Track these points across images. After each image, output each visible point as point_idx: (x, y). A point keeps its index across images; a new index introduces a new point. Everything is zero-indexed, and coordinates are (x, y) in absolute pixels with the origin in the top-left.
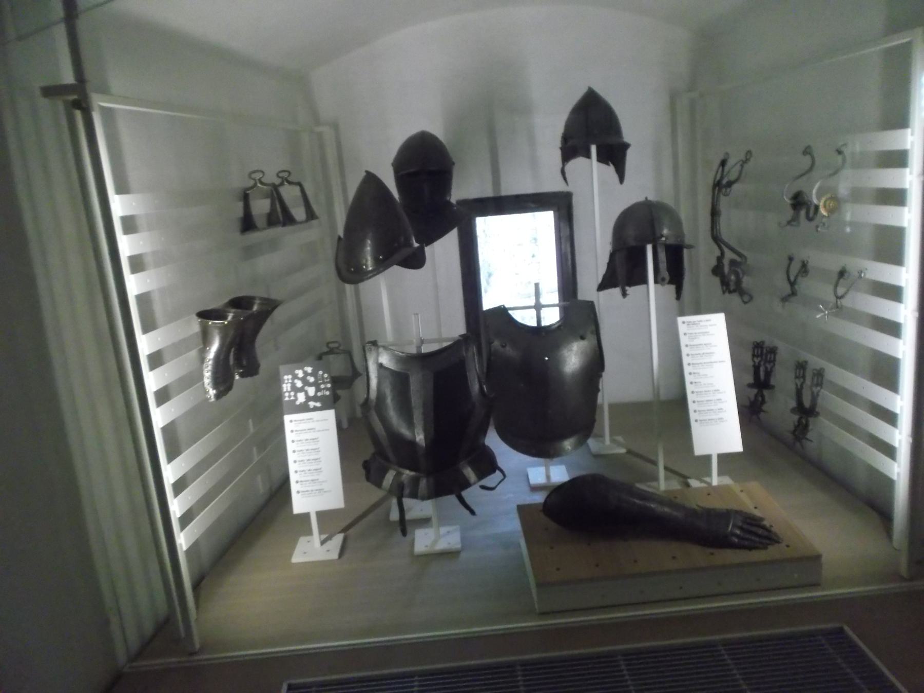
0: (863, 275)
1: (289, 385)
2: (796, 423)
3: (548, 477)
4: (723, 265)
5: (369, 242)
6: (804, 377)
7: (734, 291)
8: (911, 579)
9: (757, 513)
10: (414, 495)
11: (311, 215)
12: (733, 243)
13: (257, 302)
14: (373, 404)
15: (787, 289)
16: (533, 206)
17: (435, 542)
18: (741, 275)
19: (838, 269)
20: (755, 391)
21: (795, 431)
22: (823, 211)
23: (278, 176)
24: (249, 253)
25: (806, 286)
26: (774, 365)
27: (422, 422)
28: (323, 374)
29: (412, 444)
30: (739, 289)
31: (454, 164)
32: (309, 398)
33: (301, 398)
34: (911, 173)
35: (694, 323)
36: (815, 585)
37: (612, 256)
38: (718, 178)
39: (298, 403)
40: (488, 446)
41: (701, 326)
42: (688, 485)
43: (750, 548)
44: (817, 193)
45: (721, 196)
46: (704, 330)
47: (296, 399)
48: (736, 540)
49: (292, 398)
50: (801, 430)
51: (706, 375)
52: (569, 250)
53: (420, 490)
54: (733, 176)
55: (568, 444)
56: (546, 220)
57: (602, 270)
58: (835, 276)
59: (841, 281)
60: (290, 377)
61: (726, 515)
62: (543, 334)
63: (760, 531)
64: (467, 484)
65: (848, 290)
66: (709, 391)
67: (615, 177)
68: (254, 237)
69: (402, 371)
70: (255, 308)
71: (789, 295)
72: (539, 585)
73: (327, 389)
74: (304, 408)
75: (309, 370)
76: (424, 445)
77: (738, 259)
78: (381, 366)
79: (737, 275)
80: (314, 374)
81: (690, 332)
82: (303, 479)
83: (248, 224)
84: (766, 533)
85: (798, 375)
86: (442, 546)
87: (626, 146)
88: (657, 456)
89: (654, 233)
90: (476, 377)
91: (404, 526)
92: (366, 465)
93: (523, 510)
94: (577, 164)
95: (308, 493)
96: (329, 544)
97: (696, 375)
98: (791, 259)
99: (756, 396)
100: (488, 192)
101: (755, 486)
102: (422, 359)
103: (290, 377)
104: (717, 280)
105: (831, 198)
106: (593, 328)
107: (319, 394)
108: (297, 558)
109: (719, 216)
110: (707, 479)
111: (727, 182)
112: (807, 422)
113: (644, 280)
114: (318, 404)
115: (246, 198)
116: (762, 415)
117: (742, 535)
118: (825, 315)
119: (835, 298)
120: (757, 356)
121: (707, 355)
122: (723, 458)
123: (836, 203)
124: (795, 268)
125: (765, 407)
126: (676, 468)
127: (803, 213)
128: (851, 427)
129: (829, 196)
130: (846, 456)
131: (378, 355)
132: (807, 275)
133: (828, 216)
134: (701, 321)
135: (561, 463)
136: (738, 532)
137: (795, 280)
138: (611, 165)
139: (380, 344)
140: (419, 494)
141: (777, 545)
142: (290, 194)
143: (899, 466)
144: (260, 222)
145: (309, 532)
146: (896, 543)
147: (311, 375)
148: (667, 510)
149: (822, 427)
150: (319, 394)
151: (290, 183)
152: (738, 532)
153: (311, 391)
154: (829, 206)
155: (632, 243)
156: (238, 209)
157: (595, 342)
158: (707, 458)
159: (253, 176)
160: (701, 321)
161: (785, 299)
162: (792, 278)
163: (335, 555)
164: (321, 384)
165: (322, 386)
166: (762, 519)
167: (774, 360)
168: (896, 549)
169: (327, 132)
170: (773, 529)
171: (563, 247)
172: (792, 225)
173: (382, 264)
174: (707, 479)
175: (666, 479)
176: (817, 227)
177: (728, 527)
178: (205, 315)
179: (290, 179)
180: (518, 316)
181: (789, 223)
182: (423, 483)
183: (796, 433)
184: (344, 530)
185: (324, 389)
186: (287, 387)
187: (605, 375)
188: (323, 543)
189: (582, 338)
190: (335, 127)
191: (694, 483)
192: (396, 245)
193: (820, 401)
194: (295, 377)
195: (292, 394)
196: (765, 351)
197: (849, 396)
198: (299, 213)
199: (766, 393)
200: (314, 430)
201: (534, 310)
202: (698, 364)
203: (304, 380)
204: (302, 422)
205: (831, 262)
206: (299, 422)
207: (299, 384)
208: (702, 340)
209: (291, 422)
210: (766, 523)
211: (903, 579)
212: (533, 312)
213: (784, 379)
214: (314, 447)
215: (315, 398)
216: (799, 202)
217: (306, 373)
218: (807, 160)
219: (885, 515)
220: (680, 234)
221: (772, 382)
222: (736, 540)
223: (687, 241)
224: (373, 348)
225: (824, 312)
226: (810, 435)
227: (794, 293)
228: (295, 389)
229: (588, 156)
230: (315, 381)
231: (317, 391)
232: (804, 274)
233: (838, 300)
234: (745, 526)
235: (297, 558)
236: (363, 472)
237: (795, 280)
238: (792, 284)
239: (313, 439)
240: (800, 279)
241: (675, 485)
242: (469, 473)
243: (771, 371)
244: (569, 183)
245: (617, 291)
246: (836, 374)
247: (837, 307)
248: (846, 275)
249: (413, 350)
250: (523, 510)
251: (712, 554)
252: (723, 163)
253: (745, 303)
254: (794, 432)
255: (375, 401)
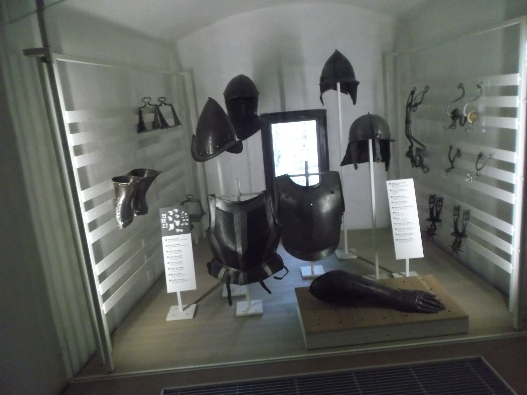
0: (492, 157)
1: (165, 220)
2: (454, 241)
3: (313, 272)
4: (413, 151)
5: (210, 138)
6: (458, 215)
7: (419, 166)
8: (520, 330)
9: (432, 292)
10: (236, 282)
11: (177, 122)
12: (418, 139)
13: (147, 172)
14: (213, 230)
15: (449, 165)
16: (304, 117)
17: (248, 309)
18: (423, 157)
19: (478, 153)
20: (431, 223)
21: (453, 246)
22: (469, 121)
23: (158, 100)
24: (142, 144)
25: (460, 163)
26: (442, 208)
27: (241, 241)
28: (184, 213)
29: (235, 253)
30: (421, 165)
31: (259, 93)
32: (176, 227)
33: (172, 227)
34: (520, 99)
35: (396, 184)
36: (465, 334)
37: (349, 146)
38: (410, 102)
39: (170, 230)
40: (278, 254)
41: (400, 186)
42: (392, 277)
43: (428, 313)
44: (466, 110)
45: (412, 112)
46: (401, 188)
47: (169, 227)
48: (420, 308)
49: (167, 227)
50: (457, 245)
51: (403, 214)
52: (324, 142)
53: (239, 279)
54: (418, 101)
55: (324, 253)
56: (311, 125)
57: (343, 154)
58: (476, 158)
59: (480, 160)
60: (165, 215)
61: (414, 294)
62: (310, 190)
63: (434, 303)
64: (266, 276)
65: (484, 166)
66: (404, 223)
67: (351, 101)
68: (145, 135)
69: (229, 211)
70: (146, 176)
71: (450, 168)
72: (308, 334)
73: (186, 222)
74: (173, 233)
75: (176, 211)
76: (242, 254)
77: (421, 148)
78: (217, 209)
79: (420, 157)
80: (179, 213)
81: (394, 189)
82: (173, 273)
83: (141, 128)
84: (437, 304)
85: (455, 214)
86: (252, 311)
87: (357, 83)
88: (375, 260)
89: (373, 133)
90: (272, 215)
91: (230, 300)
92: (209, 265)
93: (298, 291)
94: (329, 94)
95: (176, 281)
96: (188, 310)
97: (397, 214)
98: (451, 148)
99: (431, 226)
100: (279, 110)
101: (430, 277)
102: (241, 205)
103: (165, 215)
104: (409, 160)
105: (474, 113)
106: (338, 187)
107: (182, 225)
108: (169, 318)
109: (410, 123)
110: (403, 273)
111: (415, 104)
112: (460, 241)
113: (367, 160)
114: (182, 231)
115: (140, 113)
116: (434, 237)
117: (423, 305)
118: (471, 179)
119: (476, 170)
120: (432, 203)
121: (403, 202)
122: (413, 261)
123: (477, 116)
124: (454, 153)
125: (436, 232)
126: (386, 267)
127: (458, 121)
128: (485, 244)
129: (473, 111)
130: (483, 260)
131: (216, 202)
132: (460, 157)
133: (472, 123)
134: (400, 183)
135: (320, 264)
136: (421, 303)
137: (454, 160)
138: (349, 94)
139: (216, 196)
140: (239, 282)
141: (443, 311)
142: (165, 110)
143: (513, 266)
144: (148, 126)
145: (176, 303)
146: (511, 310)
147: (177, 214)
148: (380, 290)
149: (469, 243)
150: (182, 225)
151: (165, 104)
152: (421, 303)
153: (178, 223)
154: (473, 117)
155: (360, 138)
156: (136, 119)
157: (339, 195)
158: (403, 261)
159: (145, 100)
160: (400, 183)
161: (448, 171)
162: (452, 159)
163: (191, 317)
164: (183, 219)
165: (184, 220)
166: (434, 296)
167: (442, 205)
168: (511, 313)
169: (187, 75)
170: (441, 302)
171: (321, 141)
172: (452, 128)
173: (218, 151)
174: (403, 273)
175: (380, 273)
176: (466, 129)
177: (415, 300)
178: (117, 180)
179: (165, 102)
180: (295, 180)
181: (450, 127)
182: (241, 275)
183: (454, 247)
184: (196, 302)
185: (185, 222)
186: (164, 221)
187: (345, 214)
188: (184, 309)
189: (332, 193)
190: (191, 72)
191: (396, 275)
192: (226, 140)
193: (467, 228)
194: (168, 215)
195: (167, 224)
196: (436, 200)
197: (484, 226)
198: (170, 121)
199: (437, 224)
200: (179, 245)
201: (304, 176)
202: (398, 207)
203: (173, 217)
204: (172, 240)
205: (474, 149)
206: (171, 240)
207: (171, 219)
208: (401, 194)
209: (166, 241)
210: (437, 298)
211: (515, 330)
212: (304, 178)
213: (447, 216)
214: (179, 255)
215: (180, 227)
216: (456, 115)
217: (174, 213)
218: (460, 91)
219: (505, 293)
220: (388, 134)
221: (441, 218)
222: (420, 308)
223: (392, 137)
224: (213, 198)
225: (470, 178)
226: (462, 248)
227: (453, 167)
228: (168, 222)
229: (336, 89)
230: (180, 217)
231: (181, 223)
232: (458, 156)
233: (478, 171)
234: (425, 300)
235: (169, 318)
236: (207, 269)
237: (454, 160)
238: (452, 162)
239: (179, 250)
240: (456, 159)
241: (385, 276)
242: (268, 270)
243: (440, 211)
244: (324, 104)
245: (352, 166)
246: (477, 213)
247: (478, 175)
248: (483, 157)
249: (235, 200)
250: (298, 291)
251: (406, 316)
252: (412, 93)
253: (425, 173)
254: (453, 246)
255: (214, 228)
